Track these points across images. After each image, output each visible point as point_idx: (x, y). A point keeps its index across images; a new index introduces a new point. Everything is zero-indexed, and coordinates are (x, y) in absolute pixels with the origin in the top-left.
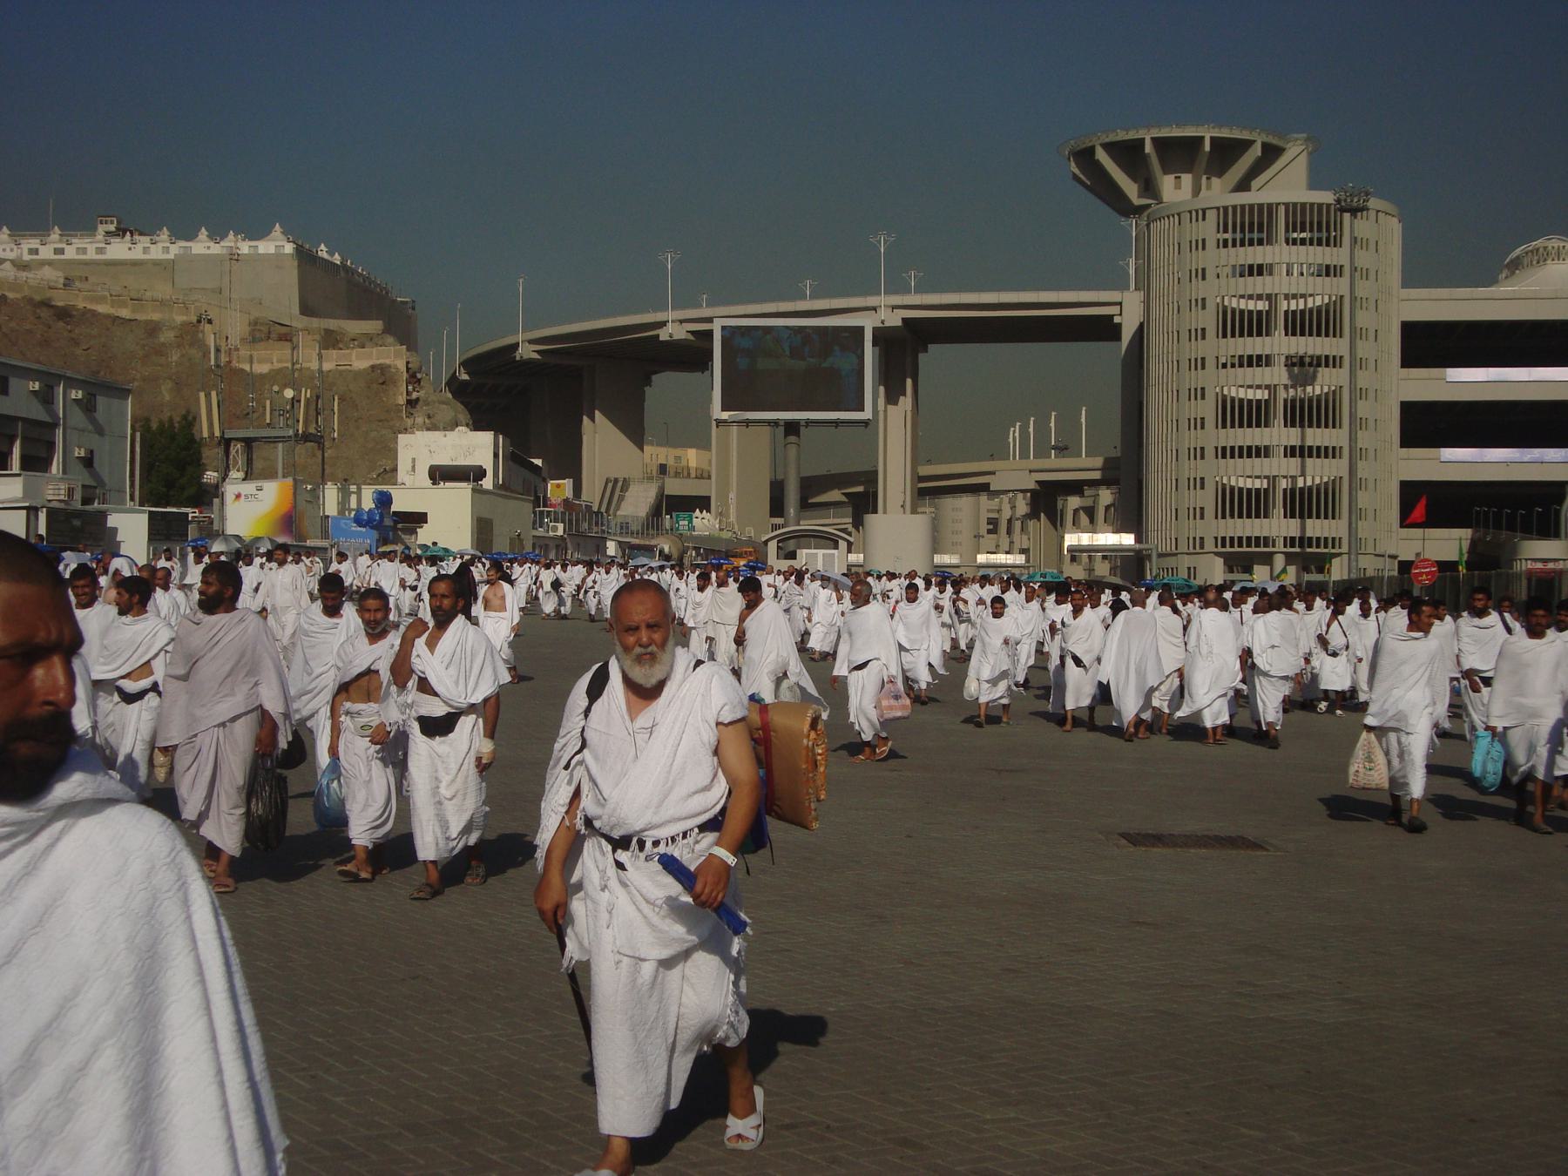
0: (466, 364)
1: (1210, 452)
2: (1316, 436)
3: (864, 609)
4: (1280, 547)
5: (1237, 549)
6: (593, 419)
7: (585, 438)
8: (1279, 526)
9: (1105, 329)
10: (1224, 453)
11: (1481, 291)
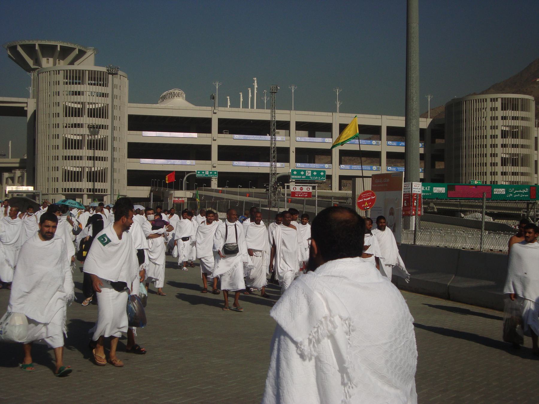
2: (99, 153)
4: (85, 192)
8: (85, 185)
9: (21, 112)
10: (66, 158)
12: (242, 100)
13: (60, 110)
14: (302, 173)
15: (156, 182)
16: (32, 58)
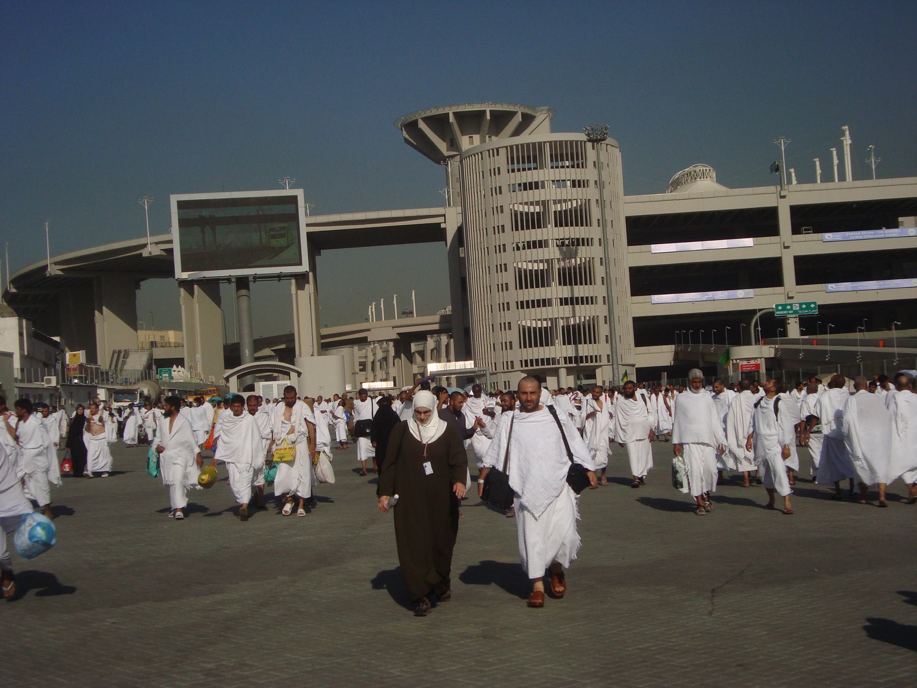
0: (14, 282)
1: (513, 306)
2: (580, 291)
3: (566, 470)
4: (562, 364)
5: (535, 367)
6: (101, 312)
7: (97, 325)
8: (560, 350)
9: (434, 233)
10: (522, 305)
11: (668, 195)
12: (819, 171)
13: (505, 219)
14: (788, 307)
15: (686, 335)
16: (443, 139)
